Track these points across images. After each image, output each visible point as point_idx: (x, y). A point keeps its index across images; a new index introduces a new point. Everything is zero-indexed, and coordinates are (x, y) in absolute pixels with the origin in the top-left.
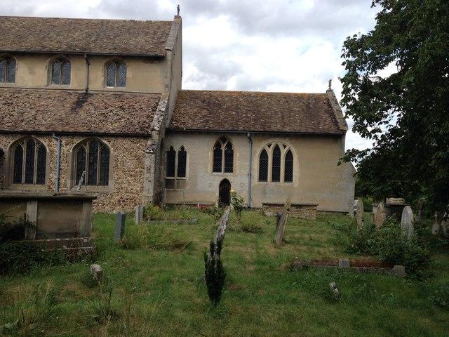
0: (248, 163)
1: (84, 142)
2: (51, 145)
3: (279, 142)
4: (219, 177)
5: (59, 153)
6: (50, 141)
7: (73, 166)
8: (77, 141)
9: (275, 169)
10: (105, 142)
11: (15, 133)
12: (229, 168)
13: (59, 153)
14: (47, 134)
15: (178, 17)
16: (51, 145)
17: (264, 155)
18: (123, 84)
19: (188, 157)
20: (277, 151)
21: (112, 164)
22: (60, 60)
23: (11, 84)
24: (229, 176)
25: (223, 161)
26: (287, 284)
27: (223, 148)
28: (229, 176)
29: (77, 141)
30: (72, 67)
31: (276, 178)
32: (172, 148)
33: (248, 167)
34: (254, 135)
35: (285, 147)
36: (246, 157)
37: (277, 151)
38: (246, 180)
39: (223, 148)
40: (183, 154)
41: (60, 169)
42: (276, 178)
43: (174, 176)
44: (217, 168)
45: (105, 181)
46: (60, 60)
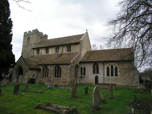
0: (103, 71)
1: (56, 66)
2: (49, 67)
3: (113, 64)
4: (94, 75)
5: (51, 69)
6: (49, 66)
7: (54, 73)
8: (54, 66)
9: (111, 72)
10: (60, 66)
11: (43, 65)
12: (98, 73)
13: (51, 69)
14: (48, 65)
16: (49, 67)
17: (108, 68)
18: (70, 51)
20: (112, 67)
21: (62, 72)
22: (57, 47)
23: (48, 54)
24: (97, 75)
25: (96, 70)
27: (96, 66)
28: (97, 75)
29: (54, 66)
30: (59, 49)
31: (112, 75)
32: (82, 67)
33: (103, 72)
34: (104, 62)
35: (114, 65)
36: (102, 70)
37: (112, 67)
38: (102, 76)
39: (96, 66)
40: (85, 69)
41: (51, 73)
42: (112, 75)
43: (82, 76)
44: (94, 73)
45: (60, 77)
46: (57, 47)
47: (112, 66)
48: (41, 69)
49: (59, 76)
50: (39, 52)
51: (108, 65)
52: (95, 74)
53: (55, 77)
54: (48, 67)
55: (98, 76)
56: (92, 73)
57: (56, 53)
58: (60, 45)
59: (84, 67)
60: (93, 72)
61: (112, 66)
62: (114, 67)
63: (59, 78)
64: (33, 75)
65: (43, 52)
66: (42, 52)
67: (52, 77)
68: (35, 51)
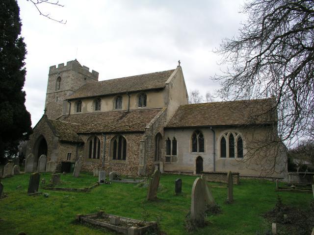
0: (212, 146)
1: (115, 137)
2: (101, 139)
3: (233, 132)
4: (195, 156)
5: (106, 142)
6: (102, 137)
7: (111, 150)
8: (112, 136)
9: (230, 149)
10: (124, 136)
11: (88, 134)
12: (202, 150)
14: (100, 134)
15: (179, 66)
16: (101, 139)
17: (223, 140)
19: (178, 143)
20: (231, 138)
21: (127, 148)
22: (118, 97)
23: (99, 111)
24: (201, 154)
25: (198, 145)
26: (252, 152)
27: (198, 136)
28: (201, 154)
29: (112, 136)
30: (123, 101)
31: (232, 155)
32: (169, 138)
33: (213, 149)
34: (216, 129)
35: (236, 134)
36: (212, 145)
37: (231, 138)
38: (212, 157)
39: (198, 136)
40: (175, 142)
41: (105, 151)
42: (232, 155)
44: (194, 150)
45: (124, 159)
46: (118, 97)
47: (231, 136)
48: (86, 142)
49: (122, 157)
50: (81, 108)
51: (222, 134)
52: (196, 153)
53: (114, 158)
54: (99, 137)
55: (202, 157)
56: (189, 151)
57: (116, 110)
58: (124, 93)
59: (175, 138)
60: (193, 148)
61: (231, 136)
62: (236, 138)
63: (122, 162)
64: (68, 154)
65: (89, 107)
66: (86, 107)
67: (108, 158)
68: (73, 105)
